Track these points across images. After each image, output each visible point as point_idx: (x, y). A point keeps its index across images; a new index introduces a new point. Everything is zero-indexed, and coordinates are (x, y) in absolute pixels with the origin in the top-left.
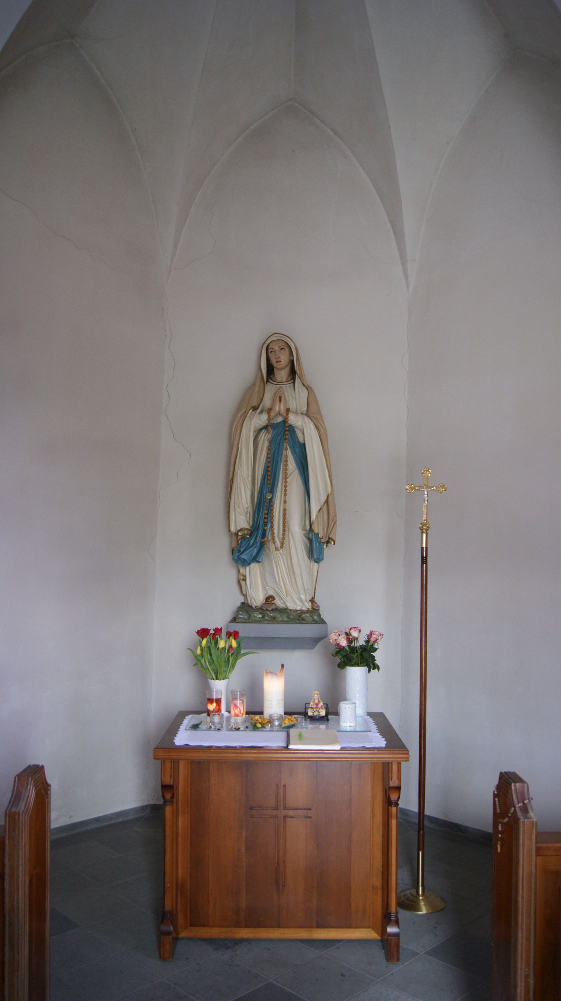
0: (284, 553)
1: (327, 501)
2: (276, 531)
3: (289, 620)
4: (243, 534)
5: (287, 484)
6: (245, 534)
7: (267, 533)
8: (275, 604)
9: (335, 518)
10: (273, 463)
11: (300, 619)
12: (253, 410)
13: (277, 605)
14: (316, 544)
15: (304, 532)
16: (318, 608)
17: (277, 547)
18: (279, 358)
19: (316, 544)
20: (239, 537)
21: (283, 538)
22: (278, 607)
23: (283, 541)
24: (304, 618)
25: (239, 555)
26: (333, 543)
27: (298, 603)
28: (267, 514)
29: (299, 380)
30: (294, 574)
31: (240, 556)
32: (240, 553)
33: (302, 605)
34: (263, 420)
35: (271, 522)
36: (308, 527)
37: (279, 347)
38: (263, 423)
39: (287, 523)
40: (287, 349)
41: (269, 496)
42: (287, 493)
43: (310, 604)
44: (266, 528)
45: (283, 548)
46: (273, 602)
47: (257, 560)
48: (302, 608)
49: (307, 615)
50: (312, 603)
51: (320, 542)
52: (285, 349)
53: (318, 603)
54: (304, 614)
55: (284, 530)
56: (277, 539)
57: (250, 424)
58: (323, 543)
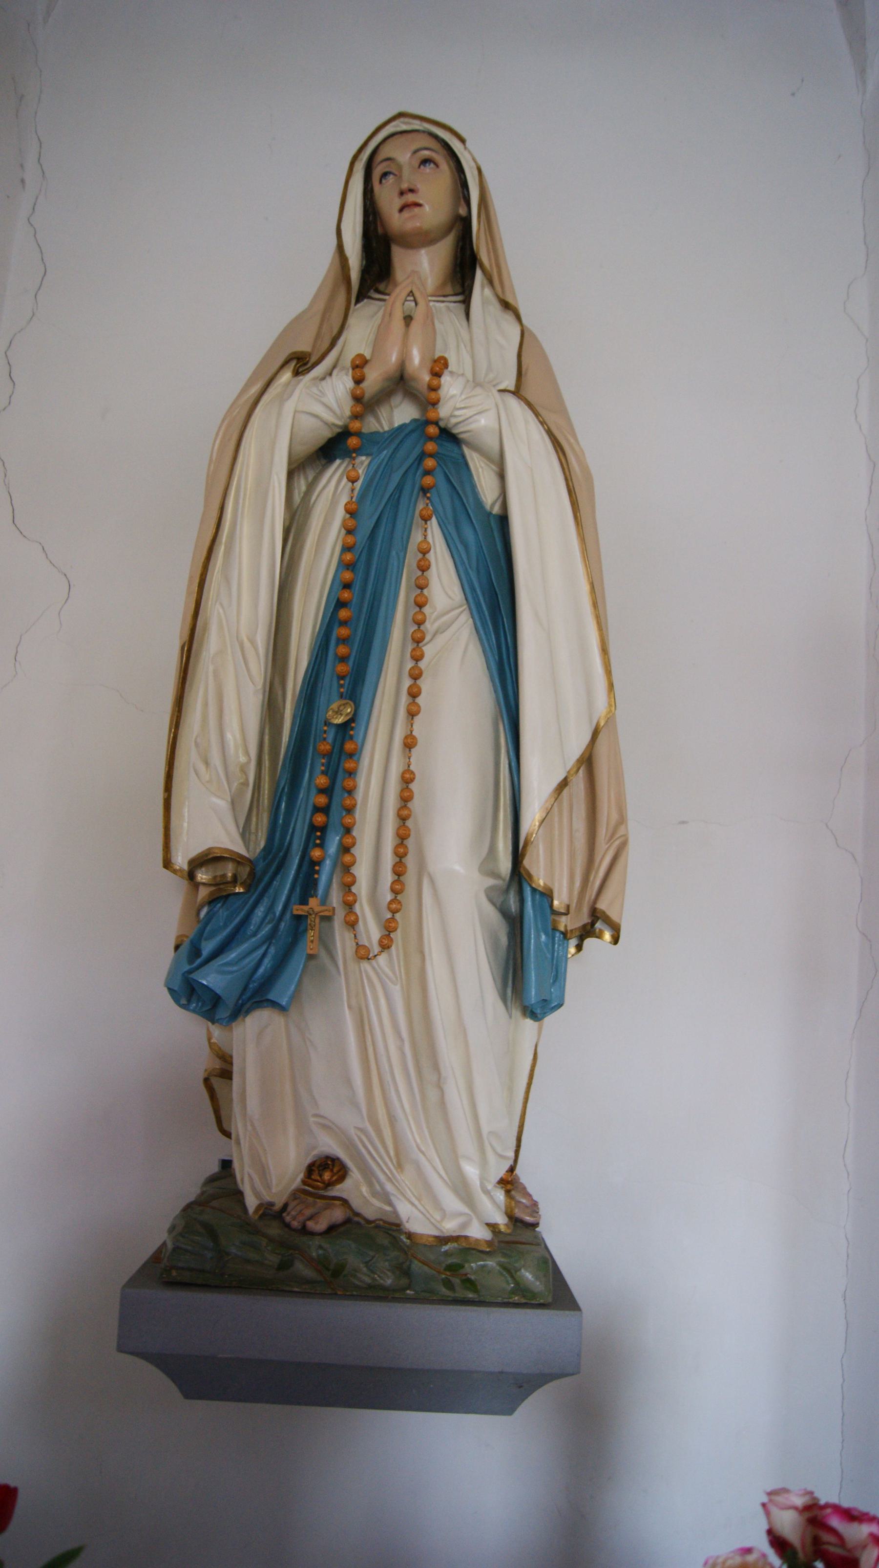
0: (394, 973)
1: (588, 761)
2: (362, 871)
3: (404, 1281)
4: (215, 878)
5: (422, 664)
6: (224, 876)
7: (323, 879)
8: (345, 1202)
9: (621, 831)
10: (364, 590)
11: (456, 1281)
12: (297, 373)
13: (356, 1204)
14: (538, 937)
15: (491, 882)
16: (531, 1216)
17: (364, 941)
18: (412, 191)
19: (538, 937)
20: (203, 892)
21: (395, 907)
22: (358, 1214)
23: (393, 918)
24: (473, 1277)
25: (190, 972)
26: (607, 936)
27: (451, 1201)
28: (327, 791)
29: (488, 292)
30: (436, 1067)
31: (194, 976)
32: (198, 961)
33: (467, 1210)
34: (330, 399)
35: (342, 830)
36: (505, 865)
37: (415, 152)
38: (330, 409)
39: (412, 833)
40: (445, 167)
41: (338, 712)
42: (420, 700)
43: (500, 1195)
44: (316, 853)
45: (393, 948)
46: (338, 1191)
47: (271, 996)
48: (465, 1225)
49: (491, 1263)
50: (508, 1192)
51: (555, 929)
52: (437, 165)
53: (530, 1190)
54: (475, 1262)
55: (399, 871)
56: (364, 909)
57: (279, 414)
58: (565, 935)
